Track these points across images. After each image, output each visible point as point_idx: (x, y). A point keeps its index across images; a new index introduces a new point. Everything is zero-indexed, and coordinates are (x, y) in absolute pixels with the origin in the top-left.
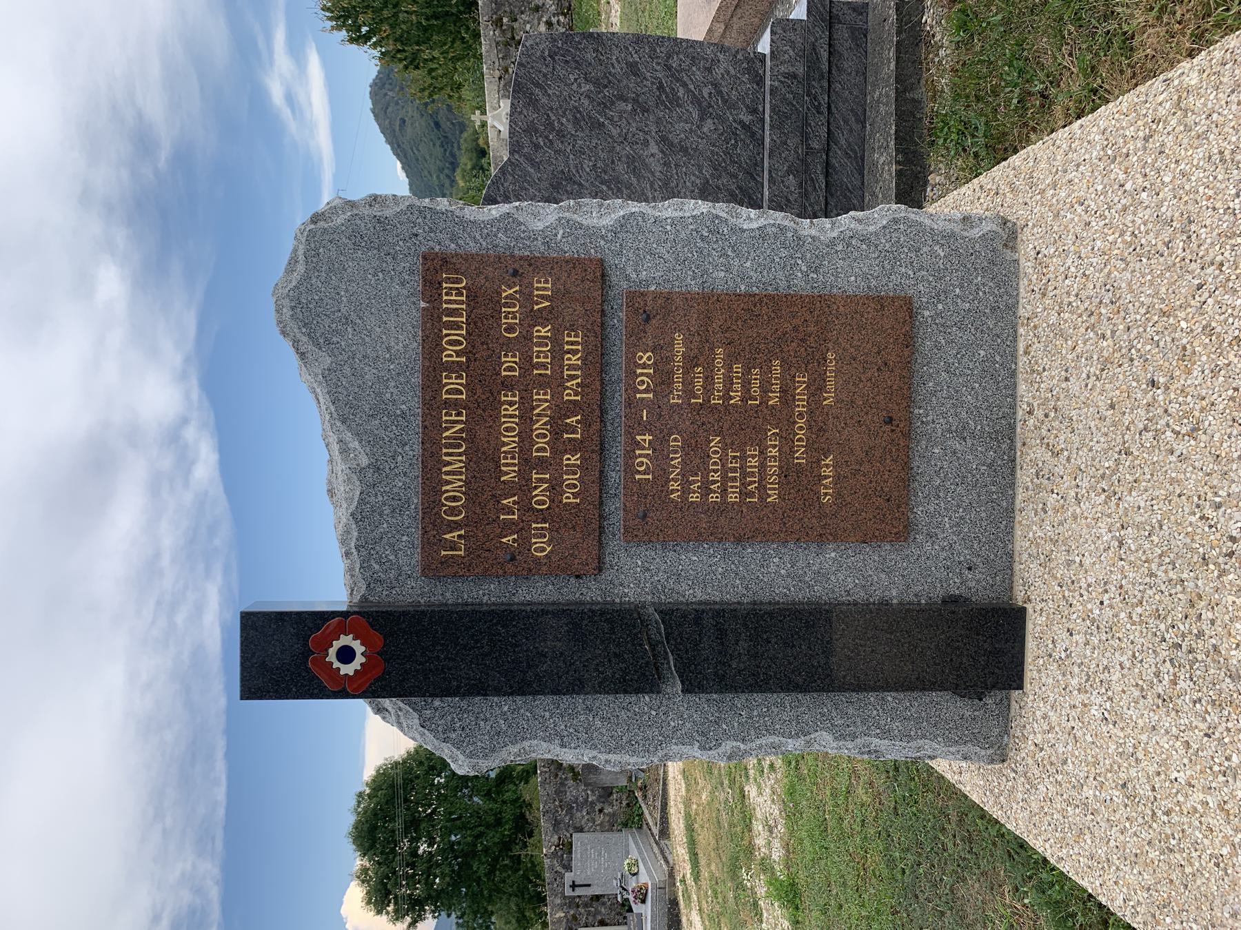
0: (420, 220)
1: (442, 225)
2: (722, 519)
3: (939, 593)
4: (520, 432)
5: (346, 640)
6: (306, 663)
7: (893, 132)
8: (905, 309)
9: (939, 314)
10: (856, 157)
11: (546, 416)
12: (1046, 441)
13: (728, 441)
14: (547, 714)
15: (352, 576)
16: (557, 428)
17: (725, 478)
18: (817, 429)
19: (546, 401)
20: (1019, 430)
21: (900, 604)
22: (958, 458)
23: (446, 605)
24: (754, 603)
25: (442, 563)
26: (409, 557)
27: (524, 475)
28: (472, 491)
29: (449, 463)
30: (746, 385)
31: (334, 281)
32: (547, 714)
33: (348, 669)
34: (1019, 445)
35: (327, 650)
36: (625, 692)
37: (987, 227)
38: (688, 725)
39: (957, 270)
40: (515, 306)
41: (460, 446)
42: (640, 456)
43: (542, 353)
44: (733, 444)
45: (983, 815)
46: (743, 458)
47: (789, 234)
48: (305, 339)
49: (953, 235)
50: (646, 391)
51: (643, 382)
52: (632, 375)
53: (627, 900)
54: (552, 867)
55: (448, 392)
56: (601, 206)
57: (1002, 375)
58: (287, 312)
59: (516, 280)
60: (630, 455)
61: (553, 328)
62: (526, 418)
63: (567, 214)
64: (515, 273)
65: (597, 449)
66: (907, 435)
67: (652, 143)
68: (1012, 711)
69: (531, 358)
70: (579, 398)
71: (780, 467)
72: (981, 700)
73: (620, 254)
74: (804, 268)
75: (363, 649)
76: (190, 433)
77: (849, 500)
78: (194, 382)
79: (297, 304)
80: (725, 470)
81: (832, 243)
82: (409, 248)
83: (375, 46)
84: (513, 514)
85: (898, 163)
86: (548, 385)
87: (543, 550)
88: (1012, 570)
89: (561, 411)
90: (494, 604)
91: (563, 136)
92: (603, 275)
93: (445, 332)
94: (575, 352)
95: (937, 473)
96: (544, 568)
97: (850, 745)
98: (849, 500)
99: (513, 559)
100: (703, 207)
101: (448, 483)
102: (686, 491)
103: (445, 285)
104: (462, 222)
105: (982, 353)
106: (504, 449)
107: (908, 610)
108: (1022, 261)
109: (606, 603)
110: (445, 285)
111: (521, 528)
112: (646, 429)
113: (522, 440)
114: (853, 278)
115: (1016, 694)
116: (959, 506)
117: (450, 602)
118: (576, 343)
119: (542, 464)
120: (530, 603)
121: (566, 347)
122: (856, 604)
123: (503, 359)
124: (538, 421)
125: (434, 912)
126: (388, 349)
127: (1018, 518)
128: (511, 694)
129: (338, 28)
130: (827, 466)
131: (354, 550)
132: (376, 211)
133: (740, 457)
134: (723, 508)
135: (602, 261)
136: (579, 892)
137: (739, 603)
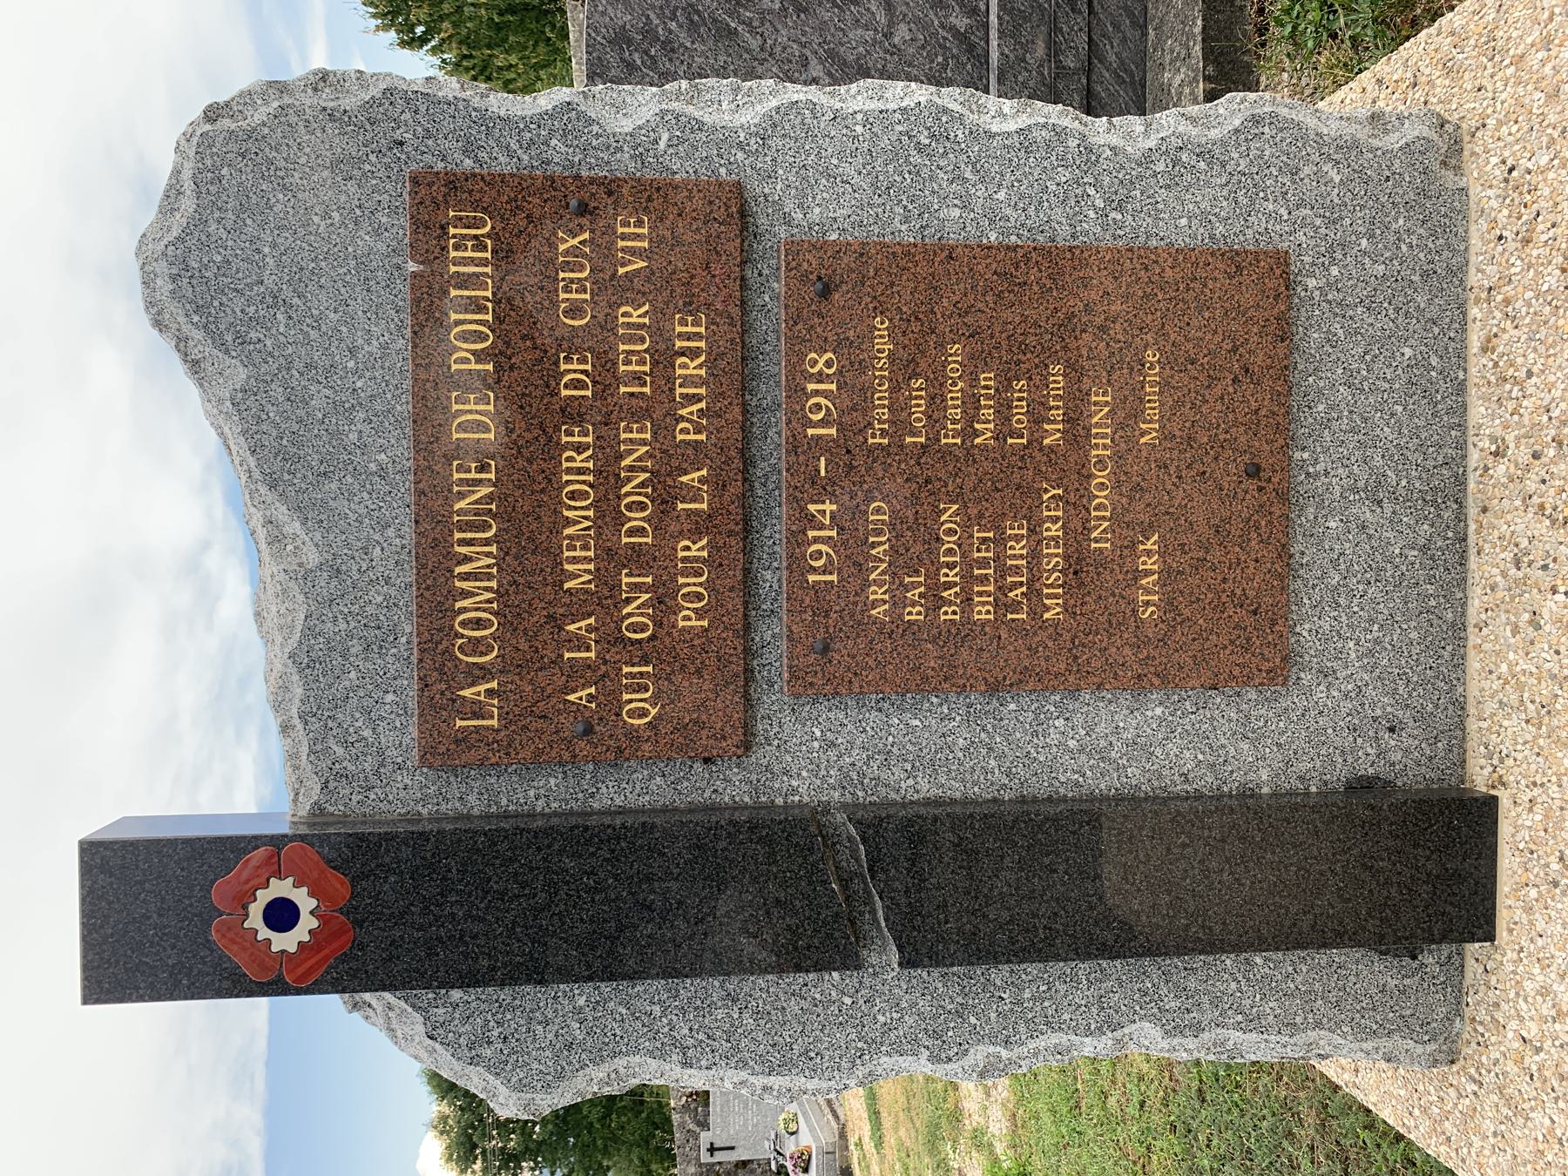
0: (407, 116)
1: (447, 125)
2: (964, 652)
3: (1339, 773)
5: (282, 888)
6: (206, 932)
7: (1198, 30)
8: (1274, 272)
9: (1333, 285)
10: (1133, 83)
11: (644, 470)
12: (1536, 500)
13: (973, 512)
14: (657, 1009)
15: (296, 768)
16: (664, 497)
17: (968, 578)
18: (1129, 487)
19: (644, 442)
20: (1472, 486)
21: (1274, 795)
22: (1370, 537)
23: (469, 817)
24: (1023, 800)
25: (457, 742)
26: (398, 732)
30: (1004, 410)
31: (251, 228)
32: (657, 1009)
33: (285, 942)
34: (1472, 511)
35: (245, 907)
36: (798, 969)
37: (1412, 131)
38: (909, 1020)
39: (1362, 207)
40: (582, 268)
42: (816, 540)
43: (632, 359)
44: (981, 516)
45: (1370, 1120)
46: (1001, 541)
47: (1073, 143)
48: (198, 335)
49: (1355, 144)
50: (823, 423)
51: (818, 407)
52: (797, 392)
53: (783, 1166)
54: (682, 1125)
55: (462, 427)
56: (736, 90)
57: (1442, 392)
58: (164, 286)
59: (585, 221)
60: (797, 539)
61: (654, 308)
62: (608, 478)
63: (675, 105)
64: (583, 209)
65: (736, 527)
66: (1283, 497)
67: (813, 62)
68: (1469, 975)
69: (615, 364)
70: (703, 437)
71: (1066, 557)
72: (1414, 958)
73: (771, 176)
74: (1100, 203)
75: (313, 903)
76: (213, 561)
77: (1187, 613)
78: (217, 495)
79: (182, 271)
80: (969, 563)
81: (1147, 158)
82: (388, 167)
83: (434, 51)
84: (588, 649)
85: (1207, 79)
86: (647, 413)
87: (643, 713)
88: (1463, 730)
89: (668, 464)
90: (555, 814)
91: (673, 50)
92: (743, 214)
94: (693, 353)
95: (1335, 563)
96: (646, 747)
97: (1191, 1043)
98: (1187, 613)
99: (589, 730)
100: (921, 93)
101: (466, 594)
102: (898, 603)
103: (452, 231)
104: (485, 121)
105: (1408, 352)
106: (567, 531)
107: (1295, 808)
108: (1475, 191)
109: (758, 807)
110: (452, 231)
111: (603, 675)
112: (824, 490)
113: (601, 515)
114: (1184, 221)
115: (1473, 948)
116: (1371, 621)
117: (476, 812)
118: (698, 336)
119: (637, 558)
120: (622, 811)
121: (678, 344)
122: (1198, 796)
123: (563, 367)
124: (629, 480)
125: (533, 1169)
126: (352, 351)
127: (1473, 639)
128: (590, 979)
129: (386, 28)
130: (1149, 553)
131: (296, 721)
132: (326, 99)
133: (994, 541)
134: (965, 632)
135: (738, 184)
136: (719, 1157)
137: (995, 800)
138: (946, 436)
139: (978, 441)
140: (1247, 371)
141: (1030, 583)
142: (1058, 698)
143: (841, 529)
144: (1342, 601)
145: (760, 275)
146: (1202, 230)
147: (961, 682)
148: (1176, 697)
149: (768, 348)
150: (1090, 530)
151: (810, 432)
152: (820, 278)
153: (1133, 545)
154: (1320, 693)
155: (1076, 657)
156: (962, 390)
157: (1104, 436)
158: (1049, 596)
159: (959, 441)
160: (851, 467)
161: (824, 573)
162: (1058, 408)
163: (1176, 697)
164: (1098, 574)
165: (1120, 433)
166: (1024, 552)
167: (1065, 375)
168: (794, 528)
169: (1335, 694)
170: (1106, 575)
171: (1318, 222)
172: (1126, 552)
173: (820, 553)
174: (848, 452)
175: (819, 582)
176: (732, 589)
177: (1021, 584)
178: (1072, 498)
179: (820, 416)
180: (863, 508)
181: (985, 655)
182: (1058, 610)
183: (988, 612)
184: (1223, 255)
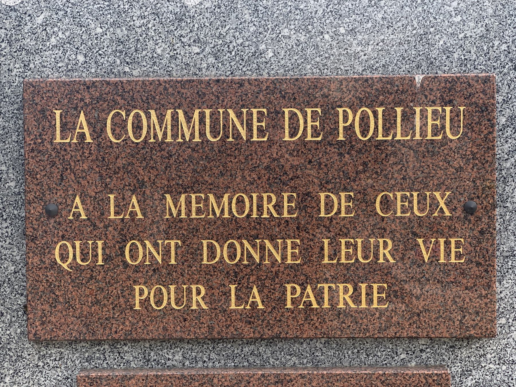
4: (245, 191)
11: (262, 258)
16: (242, 275)
19: (284, 258)
25: (43, 111)
27: (174, 227)
28: (152, 152)
29: (189, 119)
41: (215, 132)
55: (293, 116)
59: (459, 212)
62: (255, 229)
64: (469, 211)
69: (346, 235)
70: (289, 305)
82: (497, 58)
84: (117, 213)
86: (308, 261)
87: (64, 258)
89: (271, 278)
92: (469, 338)
93: (380, 110)
94: (356, 298)
96: (36, 260)
99: (50, 214)
101: (161, 118)
103: (448, 109)
106: (212, 198)
110: (448, 109)
111: (96, 224)
113: (225, 223)
118: (370, 301)
121: (363, 286)
123: (343, 195)
124: (254, 246)
126: (352, 31)
145: (422, 351)
168: (215, 381)
176: (165, 329)
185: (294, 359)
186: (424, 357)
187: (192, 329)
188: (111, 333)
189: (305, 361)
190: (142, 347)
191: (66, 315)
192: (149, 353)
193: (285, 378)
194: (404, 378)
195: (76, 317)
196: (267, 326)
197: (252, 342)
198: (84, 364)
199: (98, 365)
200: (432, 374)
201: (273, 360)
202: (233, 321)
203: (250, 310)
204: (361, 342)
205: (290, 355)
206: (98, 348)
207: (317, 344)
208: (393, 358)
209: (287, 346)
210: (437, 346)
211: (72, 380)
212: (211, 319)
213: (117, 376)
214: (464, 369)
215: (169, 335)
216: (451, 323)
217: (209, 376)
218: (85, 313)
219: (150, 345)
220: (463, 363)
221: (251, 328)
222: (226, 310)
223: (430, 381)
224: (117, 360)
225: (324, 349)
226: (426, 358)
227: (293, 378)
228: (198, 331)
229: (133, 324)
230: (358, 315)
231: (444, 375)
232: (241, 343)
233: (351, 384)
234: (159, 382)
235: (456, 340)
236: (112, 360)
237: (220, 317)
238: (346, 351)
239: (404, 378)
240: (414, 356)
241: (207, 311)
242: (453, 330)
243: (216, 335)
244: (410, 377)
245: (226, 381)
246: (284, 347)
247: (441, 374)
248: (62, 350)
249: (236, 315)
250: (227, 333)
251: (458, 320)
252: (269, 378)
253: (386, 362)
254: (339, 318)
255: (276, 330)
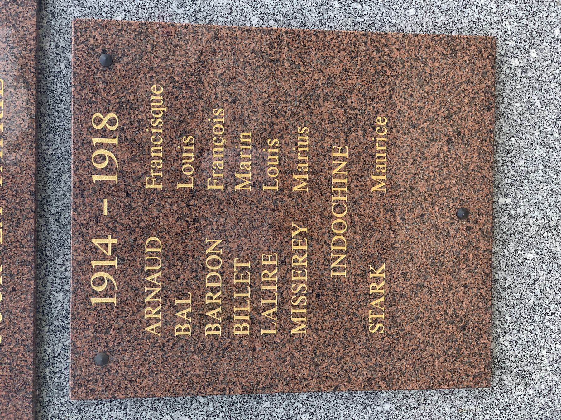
9: (532, 64)
13: (234, 245)
17: (229, 301)
19: (344, 159)
42: (99, 269)
44: (240, 249)
46: (256, 270)
50: (107, 171)
52: (84, 145)
60: (82, 268)
66: (490, 235)
71: (310, 283)
77: (408, 328)
95: (531, 287)
98: (408, 328)
102: (169, 321)
114: (412, 12)
130: (377, 280)
133: (251, 269)
134: (225, 345)
138: (211, 183)
139: (238, 187)
140: (459, 134)
141: (280, 304)
142: (305, 397)
143: (121, 260)
144: (537, 317)
145: (57, 46)
146: (426, 19)
147: (222, 386)
148: (401, 396)
149: (62, 107)
150: (330, 261)
151: (95, 178)
152: (104, 52)
153: (365, 273)
154: (519, 391)
155: (317, 365)
156: (225, 146)
157: (342, 185)
158: (296, 315)
159: (222, 187)
160: (131, 208)
161: (105, 296)
162: (304, 162)
163: (401, 396)
164: (336, 297)
165: (355, 182)
166: (276, 279)
167: (310, 136)
168: (79, 258)
169: (531, 392)
170: (343, 297)
171: (520, 14)
172: (359, 279)
173: (102, 279)
174: (128, 195)
175: (101, 304)
176: (23, 310)
177: (273, 305)
178: (315, 235)
179: (104, 165)
180: (141, 242)
181: (242, 364)
182: (303, 326)
183: (245, 328)
184: (441, 40)
185: (64, 178)
186: (64, 45)
187: (24, 283)
188: (26, 366)
189: (66, 166)
190: (48, 334)
191: (6, 412)
192: (55, 326)
193: (78, 187)
194: (78, 66)
195: (9, 402)
196: (22, 205)
197: (45, 220)
198: (65, 394)
199: (67, 379)
200: (75, 37)
201: (65, 199)
202: (16, 240)
203: (4, 223)
204: (47, 108)
205: (60, 181)
206: (48, 380)
207: (49, 153)
208: (64, 76)
209: (50, 184)
210: (52, 31)
211: (81, 405)
212: (14, 263)
213: (72, 359)
214: (76, 4)
215: (30, 307)
216: (21, 15)
217: (75, 265)
218: (4, 393)
219: (47, 325)
220: (70, 4)
221: (24, 221)
222: (4, 247)
223: (82, 39)
224: (61, 360)
225: (54, 147)
226: (64, 43)
227: (78, 180)
228: (26, 276)
229: (18, 343)
230: (11, 111)
231: (76, 25)
232: (46, 232)
233: (85, 120)
234: (79, 316)
235: (46, 11)
236: (62, 365)
237: (12, 254)
238: (56, 124)
239: (78, 66)
240: (62, 55)
241: (4, 267)
242: (29, 14)
243: (31, 258)
244: (78, 60)
245: (80, 248)
246: (52, 187)
247: (75, 28)
248: (50, 416)
249: (10, 237)
250: (29, 246)
251: (18, 8)
252: (78, 204)
253: (68, 84)
254: (14, 130)
255: (27, 196)
